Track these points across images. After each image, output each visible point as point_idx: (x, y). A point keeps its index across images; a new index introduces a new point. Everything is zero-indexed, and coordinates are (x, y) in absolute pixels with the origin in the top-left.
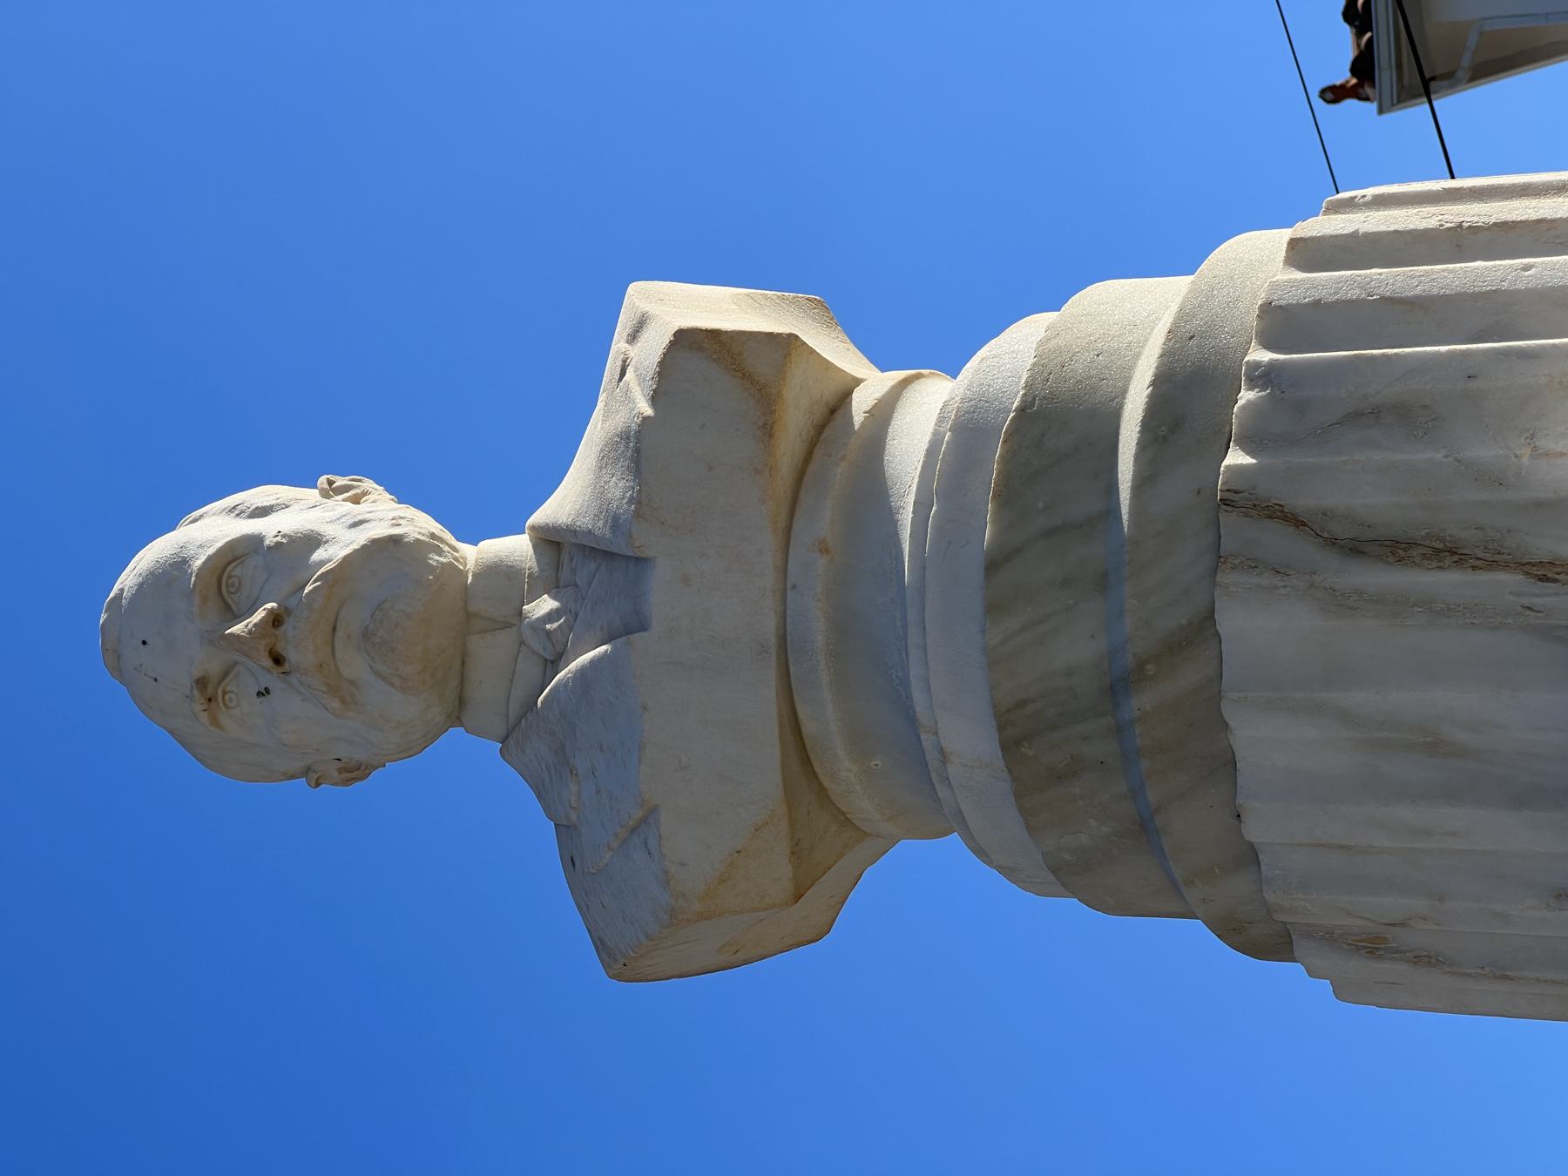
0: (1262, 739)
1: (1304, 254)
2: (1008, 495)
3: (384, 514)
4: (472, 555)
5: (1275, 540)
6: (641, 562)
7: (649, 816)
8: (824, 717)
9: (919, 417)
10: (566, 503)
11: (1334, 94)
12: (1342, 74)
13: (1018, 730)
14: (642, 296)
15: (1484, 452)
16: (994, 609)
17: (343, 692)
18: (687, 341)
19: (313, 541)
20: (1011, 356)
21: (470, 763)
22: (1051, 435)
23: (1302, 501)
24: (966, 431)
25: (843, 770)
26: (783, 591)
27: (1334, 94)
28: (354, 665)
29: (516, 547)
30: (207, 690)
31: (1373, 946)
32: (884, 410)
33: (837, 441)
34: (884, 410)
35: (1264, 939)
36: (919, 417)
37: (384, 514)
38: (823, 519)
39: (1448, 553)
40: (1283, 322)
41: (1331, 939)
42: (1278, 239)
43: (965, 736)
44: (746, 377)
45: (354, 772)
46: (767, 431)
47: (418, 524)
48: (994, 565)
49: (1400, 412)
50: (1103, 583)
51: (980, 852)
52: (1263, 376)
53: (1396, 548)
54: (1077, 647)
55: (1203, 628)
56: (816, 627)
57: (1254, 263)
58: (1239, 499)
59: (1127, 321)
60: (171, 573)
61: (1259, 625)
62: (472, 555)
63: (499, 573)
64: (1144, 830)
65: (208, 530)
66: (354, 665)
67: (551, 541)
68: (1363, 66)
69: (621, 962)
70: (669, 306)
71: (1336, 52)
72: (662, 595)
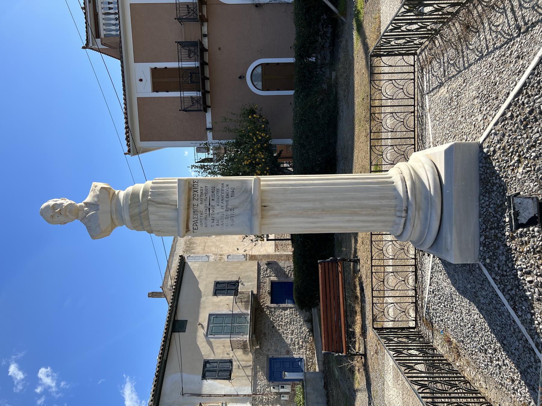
0: (151, 217)
1: (153, 183)
2: (131, 200)
3: (69, 202)
4: (78, 205)
5: (153, 203)
6: (98, 205)
7: (99, 225)
8: (114, 217)
9: (122, 194)
10: (88, 199)
11: (125, 154)
12: (127, 152)
13: (131, 217)
14: (94, 183)
15: (168, 197)
16: (130, 208)
17: (67, 216)
18: (102, 188)
19: (63, 203)
20: (130, 189)
21: (77, 222)
22: (134, 195)
23: (154, 200)
24: (127, 195)
25: (116, 221)
26: (111, 207)
27: (125, 154)
28: (68, 214)
29: (82, 204)
30: (52, 216)
31: (159, 231)
32: (118, 193)
33: (115, 197)
34: (118, 193)
35: (150, 232)
36: (122, 194)
37: (69, 202)
38: (114, 201)
39: (165, 204)
40: (152, 188)
41: (156, 231)
42: (151, 181)
43: (127, 217)
44: (107, 190)
45: (65, 223)
46: (109, 195)
47: (73, 202)
48: (130, 205)
49: (161, 194)
50: (139, 206)
51: (127, 227)
52: (151, 192)
53: (161, 204)
54: (137, 211)
55: (147, 209)
56: (114, 210)
57: (149, 183)
58: (150, 200)
59: (140, 187)
60: (48, 207)
61: (151, 209)
62: (78, 205)
63: (81, 206)
64: (142, 224)
65: (51, 202)
66: (68, 214)
67: (85, 203)
68: (129, 151)
69: (93, 237)
70: (101, 185)
71: (126, 149)
72: (100, 207)
